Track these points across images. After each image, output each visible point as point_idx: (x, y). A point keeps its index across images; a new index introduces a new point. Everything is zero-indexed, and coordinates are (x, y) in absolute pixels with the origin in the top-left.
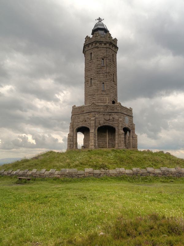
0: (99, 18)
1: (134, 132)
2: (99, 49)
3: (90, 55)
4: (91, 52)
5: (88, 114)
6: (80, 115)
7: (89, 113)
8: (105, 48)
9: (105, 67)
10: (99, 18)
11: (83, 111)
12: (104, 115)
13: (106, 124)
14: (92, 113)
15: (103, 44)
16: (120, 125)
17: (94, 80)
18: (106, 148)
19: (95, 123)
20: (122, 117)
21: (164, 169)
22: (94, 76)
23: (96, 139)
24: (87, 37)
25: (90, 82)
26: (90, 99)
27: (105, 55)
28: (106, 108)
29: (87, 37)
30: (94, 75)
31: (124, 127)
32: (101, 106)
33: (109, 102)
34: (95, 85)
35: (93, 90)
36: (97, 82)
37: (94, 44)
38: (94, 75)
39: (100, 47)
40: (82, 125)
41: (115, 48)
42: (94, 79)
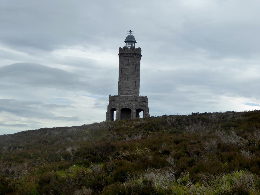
0: (130, 31)
5: (131, 101)
6: (125, 101)
7: (132, 101)
10: (130, 31)
11: (127, 99)
13: (140, 108)
14: (133, 101)
15: (137, 55)
17: (131, 78)
22: (130, 76)
25: (127, 79)
26: (127, 90)
27: (137, 63)
34: (131, 82)
37: (134, 55)
40: (126, 107)
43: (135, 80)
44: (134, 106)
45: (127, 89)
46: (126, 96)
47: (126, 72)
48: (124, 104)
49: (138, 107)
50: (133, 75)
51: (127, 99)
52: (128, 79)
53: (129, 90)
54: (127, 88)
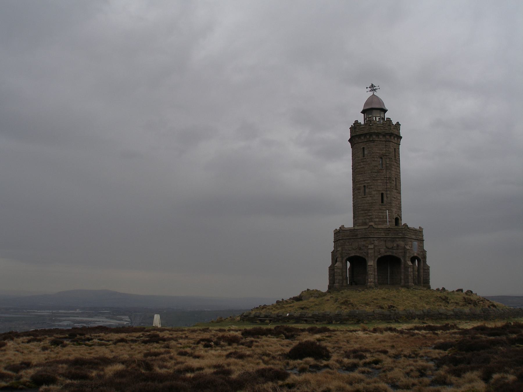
0: (372, 85)
1: (426, 262)
3: (362, 150)
6: (352, 240)
10: (372, 85)
11: (356, 235)
12: (385, 241)
13: (388, 254)
16: (408, 255)
18: (387, 284)
19: (374, 252)
20: (410, 243)
22: (369, 183)
23: (376, 274)
24: (356, 122)
25: (362, 191)
28: (388, 232)
29: (356, 122)
30: (369, 181)
31: (412, 256)
36: (374, 193)
37: (368, 137)
38: (369, 181)
41: (398, 139)
43: (379, 191)
44: (370, 251)
45: (363, 212)
49: (382, 250)
50: (374, 180)
51: (356, 235)
52: (365, 190)
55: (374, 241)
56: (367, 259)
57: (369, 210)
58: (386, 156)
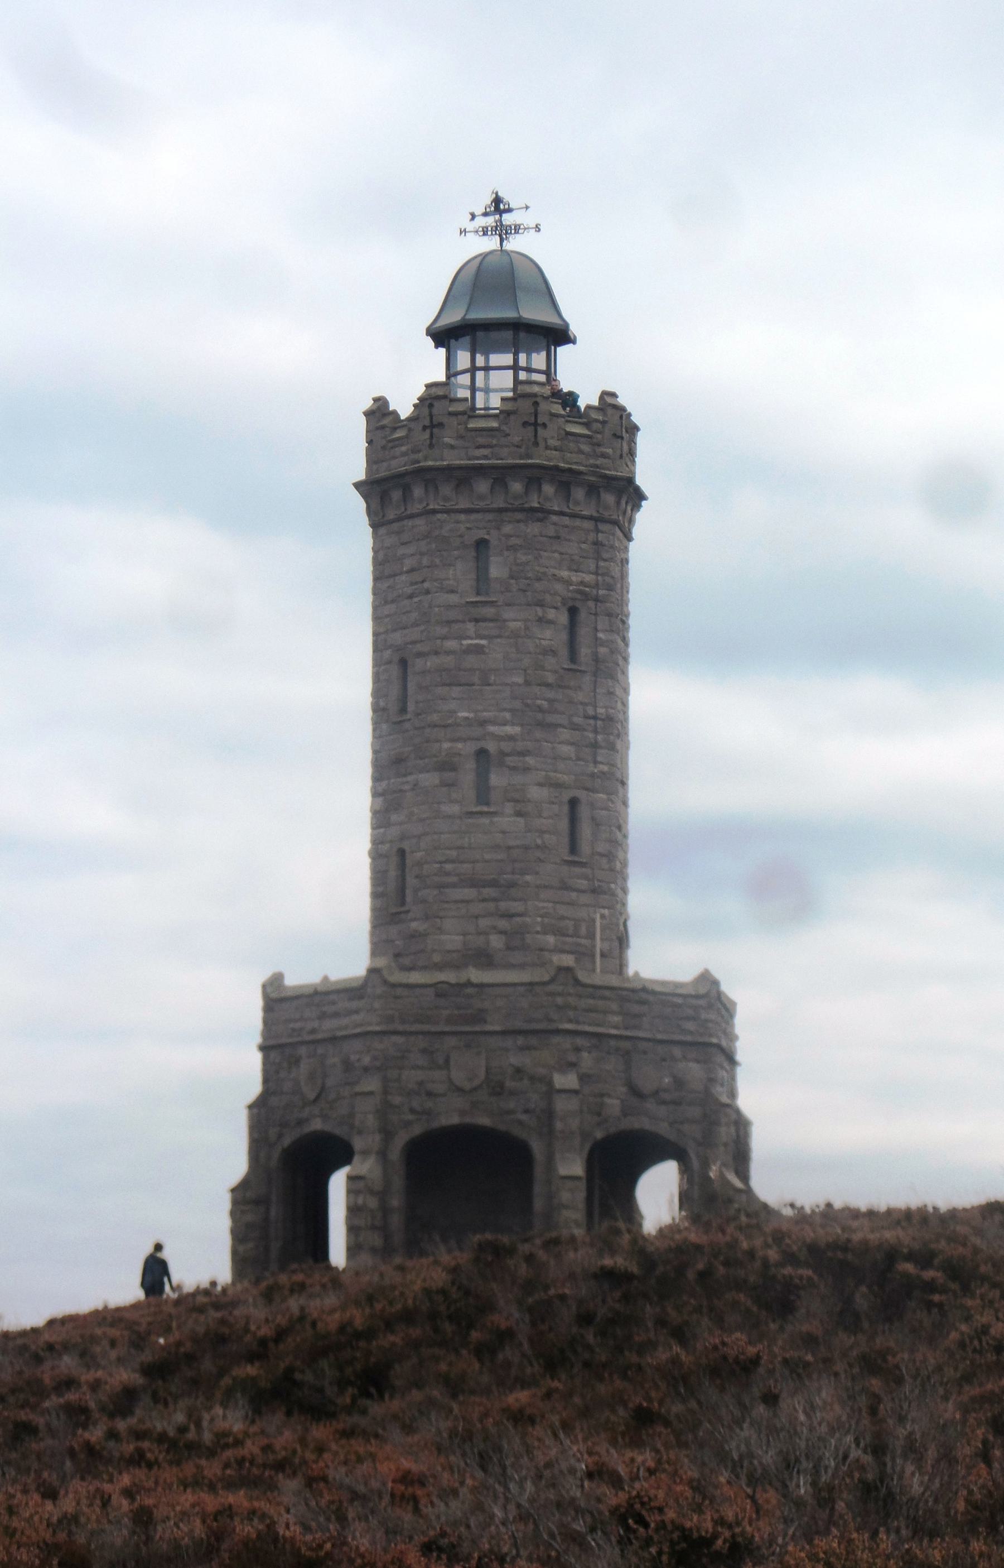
0: (497, 200)
2: (551, 531)
4: (482, 534)
5: (520, 1041)
6: (452, 1041)
7: (533, 1041)
8: (590, 518)
9: (587, 679)
11: (479, 1017)
14: (556, 1039)
17: (514, 769)
21: (31, 1417)
22: (511, 738)
25: (467, 777)
26: (477, 908)
27: (589, 578)
30: (509, 730)
32: (607, 993)
33: (606, 946)
34: (519, 814)
35: (496, 847)
36: (536, 793)
38: (509, 730)
39: (562, 513)
42: (510, 761)
43: (558, 786)
46: (469, 984)
47: (456, 691)
48: (438, 1075)
49: (613, 1105)
51: (479, 1017)
53: (503, 905)
54: (473, 882)
55: (578, 1050)
56: (537, 1148)
57: (512, 885)
58: (597, 600)
